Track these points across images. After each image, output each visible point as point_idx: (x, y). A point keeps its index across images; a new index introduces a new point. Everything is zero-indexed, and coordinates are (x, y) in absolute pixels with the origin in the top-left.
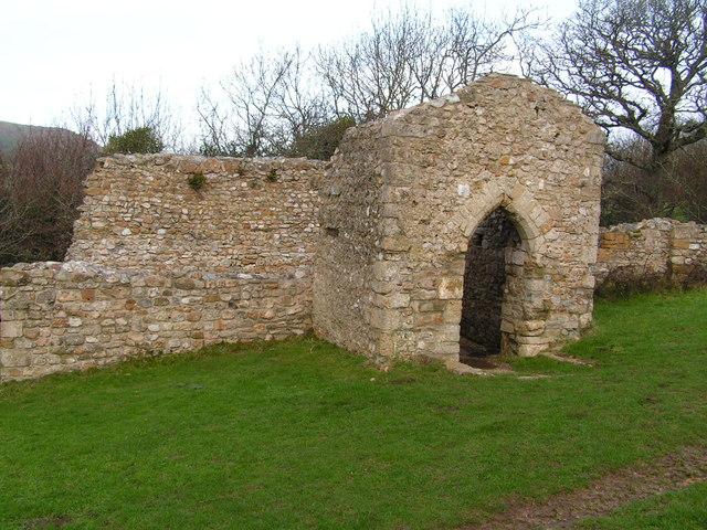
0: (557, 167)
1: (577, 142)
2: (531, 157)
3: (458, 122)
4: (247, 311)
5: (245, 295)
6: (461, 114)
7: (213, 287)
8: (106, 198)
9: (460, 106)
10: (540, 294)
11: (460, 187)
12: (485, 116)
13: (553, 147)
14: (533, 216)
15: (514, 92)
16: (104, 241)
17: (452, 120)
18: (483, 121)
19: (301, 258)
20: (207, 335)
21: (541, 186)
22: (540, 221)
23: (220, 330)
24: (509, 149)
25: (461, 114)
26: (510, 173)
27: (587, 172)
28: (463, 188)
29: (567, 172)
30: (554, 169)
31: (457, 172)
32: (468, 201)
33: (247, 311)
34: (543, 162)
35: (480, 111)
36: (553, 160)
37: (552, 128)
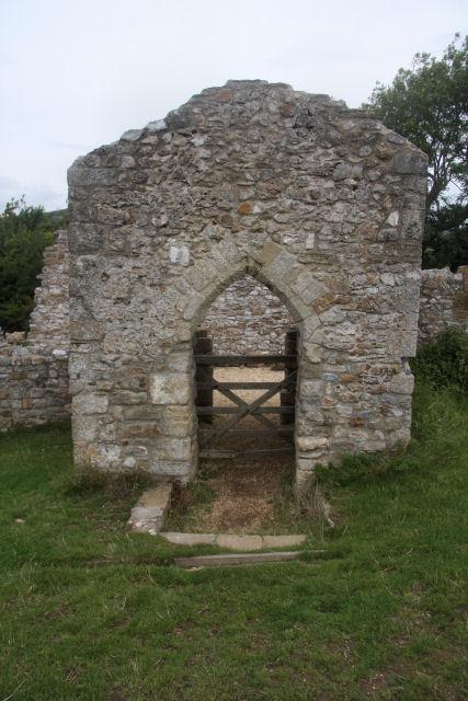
0: (338, 213)
1: (373, 174)
2: (289, 202)
3: (164, 159)
4: (55, 390)
5: (52, 373)
6: (169, 148)
7: (19, 364)
8: (61, 267)
9: (168, 136)
10: (315, 400)
11: (174, 253)
12: (207, 145)
13: (330, 184)
14: (298, 288)
15: (255, 105)
16: (60, 306)
17: (155, 158)
18: (204, 153)
19: (247, 321)
20: (16, 414)
21: (310, 243)
22: (311, 295)
23: (29, 409)
24: (252, 192)
25: (169, 148)
26: (256, 226)
27: (394, 218)
28: (177, 251)
29: (355, 220)
30: (334, 217)
31: (168, 231)
32: (188, 270)
33: (55, 390)
34: (311, 208)
35: (199, 140)
36: (331, 203)
37: (326, 154)
